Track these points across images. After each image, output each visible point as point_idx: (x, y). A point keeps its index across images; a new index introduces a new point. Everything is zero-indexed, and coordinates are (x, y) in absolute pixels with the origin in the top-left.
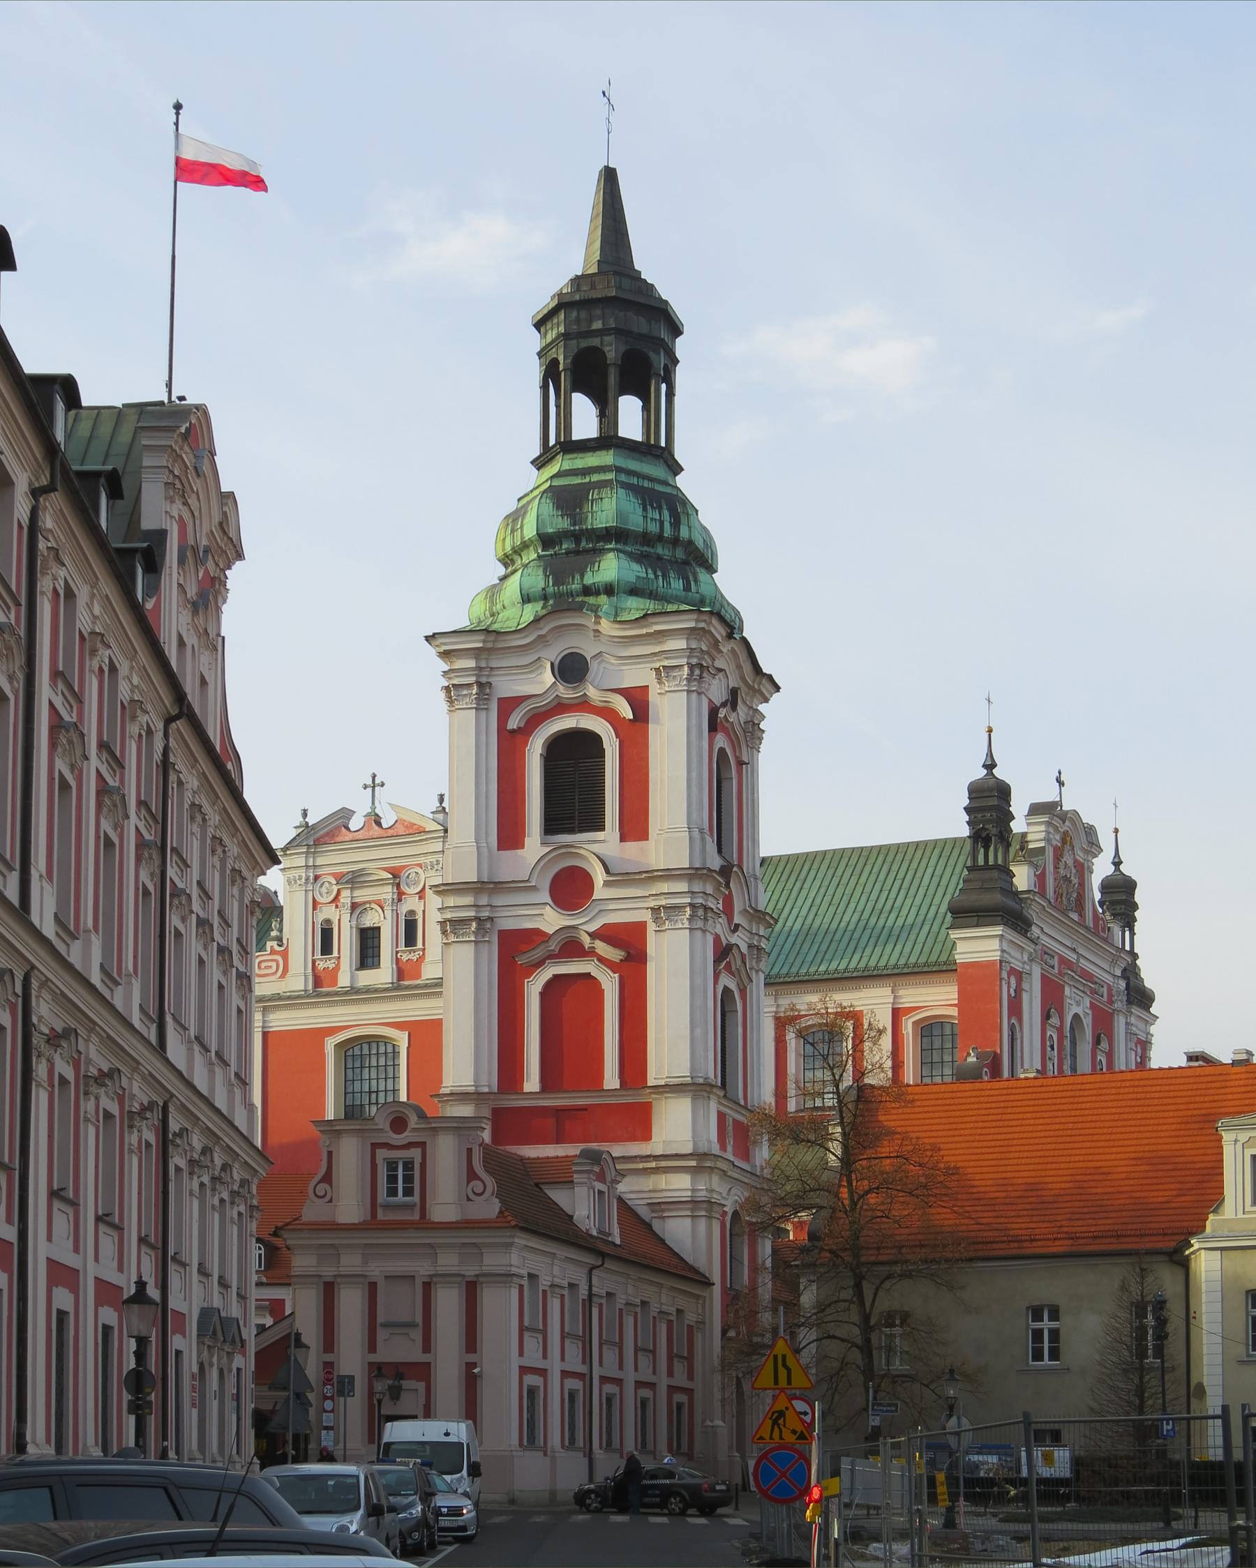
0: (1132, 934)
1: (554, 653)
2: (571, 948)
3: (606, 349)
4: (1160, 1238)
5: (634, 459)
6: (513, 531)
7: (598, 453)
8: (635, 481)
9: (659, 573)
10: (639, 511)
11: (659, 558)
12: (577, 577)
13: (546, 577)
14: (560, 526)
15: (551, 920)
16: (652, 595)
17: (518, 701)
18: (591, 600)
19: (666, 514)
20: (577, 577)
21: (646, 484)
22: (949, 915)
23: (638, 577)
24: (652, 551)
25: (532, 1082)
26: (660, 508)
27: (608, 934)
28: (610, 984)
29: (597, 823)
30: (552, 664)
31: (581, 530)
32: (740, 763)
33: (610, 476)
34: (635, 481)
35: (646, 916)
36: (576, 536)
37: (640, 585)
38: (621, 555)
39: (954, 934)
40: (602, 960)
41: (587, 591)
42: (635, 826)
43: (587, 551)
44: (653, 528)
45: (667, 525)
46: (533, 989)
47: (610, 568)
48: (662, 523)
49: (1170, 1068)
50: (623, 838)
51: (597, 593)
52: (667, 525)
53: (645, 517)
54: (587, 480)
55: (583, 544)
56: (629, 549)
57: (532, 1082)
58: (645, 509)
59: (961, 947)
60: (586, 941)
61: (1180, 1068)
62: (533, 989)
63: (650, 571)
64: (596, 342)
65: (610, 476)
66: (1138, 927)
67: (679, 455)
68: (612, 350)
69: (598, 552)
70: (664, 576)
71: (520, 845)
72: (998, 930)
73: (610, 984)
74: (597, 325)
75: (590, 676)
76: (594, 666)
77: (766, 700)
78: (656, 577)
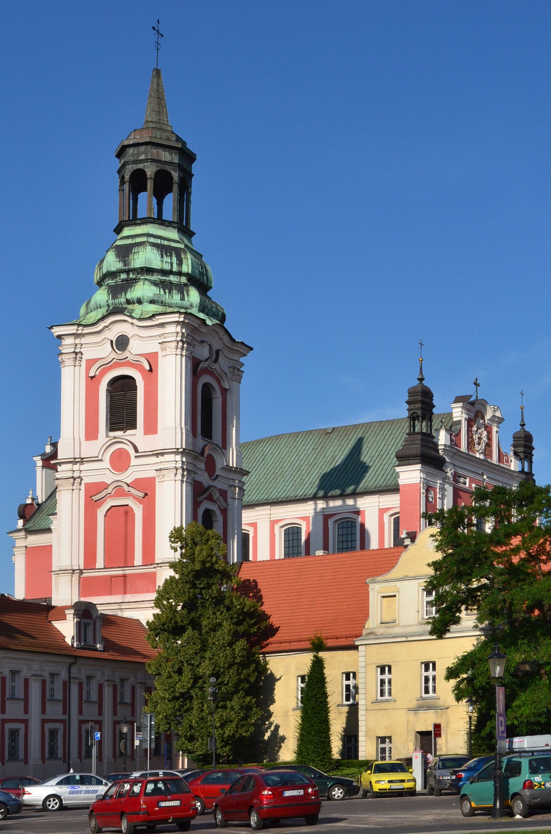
0: (531, 462)
1: (113, 333)
2: (120, 492)
3: (146, 170)
4: (298, 643)
5: (161, 229)
6: (100, 269)
7: (142, 226)
8: (158, 241)
9: (167, 291)
10: (159, 257)
11: (171, 283)
12: (123, 294)
13: (109, 294)
14: (118, 267)
15: (109, 477)
16: (163, 304)
17: (95, 361)
18: (130, 307)
19: (174, 259)
20: (123, 294)
21: (166, 243)
22: (395, 459)
23: (155, 294)
24: (167, 279)
25: (100, 563)
26: (171, 256)
27: (138, 484)
28: (138, 511)
29: (133, 426)
30: (112, 342)
31: (129, 269)
32: (224, 391)
33: (144, 239)
34: (158, 241)
35: (153, 474)
36: (128, 272)
37: (156, 298)
38: (147, 282)
39: (398, 469)
40: (135, 497)
41: (128, 302)
42: (151, 428)
43: (132, 279)
44: (167, 267)
45: (175, 265)
46: (101, 513)
47: (143, 289)
48: (172, 264)
49: (263, 561)
50: (145, 433)
51: (134, 303)
52: (175, 265)
53: (162, 261)
54: (134, 242)
55: (131, 276)
56: (153, 278)
57: (100, 563)
58: (162, 257)
59: (402, 476)
60: (126, 488)
61: (267, 561)
62: (101, 513)
63: (162, 290)
64: (141, 166)
65: (144, 239)
66: (534, 459)
67: (192, 228)
68: (150, 170)
69: (135, 281)
70: (170, 293)
71: (96, 438)
72: (419, 467)
73: (138, 511)
74: (143, 157)
75: (129, 348)
76: (131, 341)
77: (245, 355)
78: (165, 293)
